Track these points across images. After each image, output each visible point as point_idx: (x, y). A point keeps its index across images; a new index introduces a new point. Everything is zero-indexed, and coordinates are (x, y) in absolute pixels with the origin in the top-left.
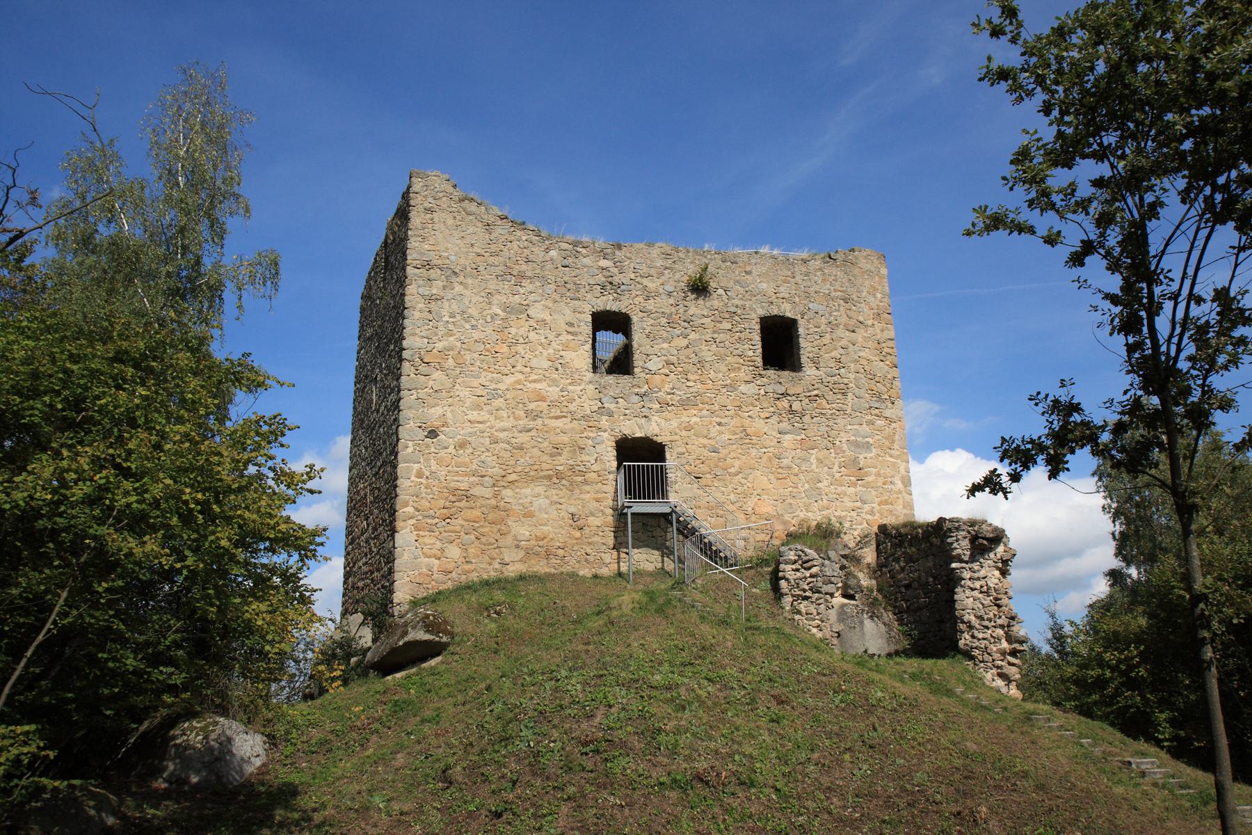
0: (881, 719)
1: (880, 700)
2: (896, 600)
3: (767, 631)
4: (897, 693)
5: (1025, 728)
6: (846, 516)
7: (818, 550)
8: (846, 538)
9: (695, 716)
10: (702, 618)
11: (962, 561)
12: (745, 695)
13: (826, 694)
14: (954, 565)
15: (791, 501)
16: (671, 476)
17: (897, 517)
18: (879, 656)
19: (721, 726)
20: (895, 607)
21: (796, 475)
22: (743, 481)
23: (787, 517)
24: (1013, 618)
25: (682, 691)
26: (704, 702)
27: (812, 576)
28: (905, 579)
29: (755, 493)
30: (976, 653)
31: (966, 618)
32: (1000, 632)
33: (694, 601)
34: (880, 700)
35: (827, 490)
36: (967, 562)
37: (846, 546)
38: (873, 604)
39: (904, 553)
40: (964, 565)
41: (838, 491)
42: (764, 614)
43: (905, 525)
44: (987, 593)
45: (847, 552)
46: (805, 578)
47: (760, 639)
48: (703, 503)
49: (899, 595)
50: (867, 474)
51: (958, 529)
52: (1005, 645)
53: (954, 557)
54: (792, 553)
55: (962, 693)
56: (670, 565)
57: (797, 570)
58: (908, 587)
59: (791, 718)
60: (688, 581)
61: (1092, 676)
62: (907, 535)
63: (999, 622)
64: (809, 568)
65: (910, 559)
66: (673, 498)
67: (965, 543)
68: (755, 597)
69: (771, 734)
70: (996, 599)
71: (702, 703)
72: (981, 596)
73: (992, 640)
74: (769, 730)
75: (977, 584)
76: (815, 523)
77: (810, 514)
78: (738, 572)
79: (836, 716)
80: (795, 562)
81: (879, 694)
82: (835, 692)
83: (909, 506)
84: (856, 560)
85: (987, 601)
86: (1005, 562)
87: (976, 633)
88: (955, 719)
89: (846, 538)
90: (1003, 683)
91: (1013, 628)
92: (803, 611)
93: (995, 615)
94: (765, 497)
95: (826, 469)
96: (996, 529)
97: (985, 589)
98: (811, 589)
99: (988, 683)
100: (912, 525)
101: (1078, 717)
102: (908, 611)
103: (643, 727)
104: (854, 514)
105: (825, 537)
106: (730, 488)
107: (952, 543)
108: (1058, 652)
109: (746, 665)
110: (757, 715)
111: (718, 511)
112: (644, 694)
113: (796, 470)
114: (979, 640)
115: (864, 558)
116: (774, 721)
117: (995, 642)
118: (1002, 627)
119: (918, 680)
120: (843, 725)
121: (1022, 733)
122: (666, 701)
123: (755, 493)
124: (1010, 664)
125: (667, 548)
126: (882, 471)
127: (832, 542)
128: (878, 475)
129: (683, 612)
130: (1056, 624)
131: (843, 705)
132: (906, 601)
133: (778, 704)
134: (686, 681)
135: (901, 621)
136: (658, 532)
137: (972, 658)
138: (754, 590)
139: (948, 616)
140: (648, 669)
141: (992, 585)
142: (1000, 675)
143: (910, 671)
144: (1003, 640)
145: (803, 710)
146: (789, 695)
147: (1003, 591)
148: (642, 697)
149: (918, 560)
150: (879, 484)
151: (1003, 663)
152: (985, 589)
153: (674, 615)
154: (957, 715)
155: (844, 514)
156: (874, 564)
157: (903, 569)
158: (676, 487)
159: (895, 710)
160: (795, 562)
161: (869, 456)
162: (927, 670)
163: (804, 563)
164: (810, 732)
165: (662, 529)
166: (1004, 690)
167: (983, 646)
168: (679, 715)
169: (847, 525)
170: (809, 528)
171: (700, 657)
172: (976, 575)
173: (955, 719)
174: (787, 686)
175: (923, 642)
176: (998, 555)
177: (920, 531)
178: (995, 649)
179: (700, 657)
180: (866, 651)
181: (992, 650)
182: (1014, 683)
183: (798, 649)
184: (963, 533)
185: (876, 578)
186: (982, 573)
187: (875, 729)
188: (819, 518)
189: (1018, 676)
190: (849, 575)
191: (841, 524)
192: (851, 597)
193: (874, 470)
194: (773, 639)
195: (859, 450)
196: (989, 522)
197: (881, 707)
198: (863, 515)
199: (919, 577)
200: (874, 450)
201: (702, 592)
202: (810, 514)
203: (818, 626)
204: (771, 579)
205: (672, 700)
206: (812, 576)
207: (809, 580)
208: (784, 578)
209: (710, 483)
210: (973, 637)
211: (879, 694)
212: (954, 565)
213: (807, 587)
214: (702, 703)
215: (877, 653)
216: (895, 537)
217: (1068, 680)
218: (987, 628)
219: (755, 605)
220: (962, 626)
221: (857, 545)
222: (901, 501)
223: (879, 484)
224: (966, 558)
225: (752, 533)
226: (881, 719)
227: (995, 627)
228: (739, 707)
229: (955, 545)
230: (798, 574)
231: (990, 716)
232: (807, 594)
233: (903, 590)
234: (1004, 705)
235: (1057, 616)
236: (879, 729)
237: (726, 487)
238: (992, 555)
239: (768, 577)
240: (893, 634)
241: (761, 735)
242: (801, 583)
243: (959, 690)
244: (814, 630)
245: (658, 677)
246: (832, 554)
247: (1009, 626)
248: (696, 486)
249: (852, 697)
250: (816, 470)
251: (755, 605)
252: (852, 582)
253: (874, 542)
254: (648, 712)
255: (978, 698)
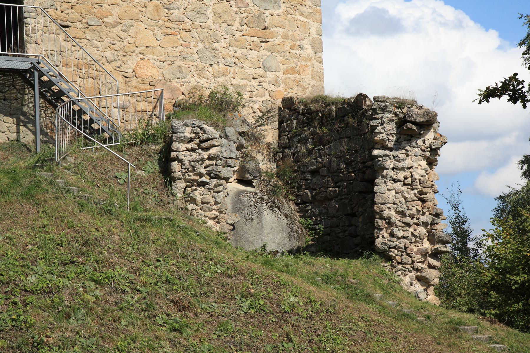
0: (296, 327)
1: (293, 306)
2: (299, 187)
3: (159, 222)
4: (313, 298)
5: (452, 340)
6: (245, 85)
7: (215, 125)
8: (244, 112)
9: (83, 325)
10: (81, 205)
11: (385, 148)
12: (139, 299)
13: (232, 298)
14: (376, 152)
15: (181, 63)
16: (30, 22)
17: (304, 89)
18: (283, 253)
19: (115, 337)
20: (297, 196)
21: (188, 31)
22: (123, 35)
23: (176, 83)
24: (437, 215)
25: (65, 295)
26: (92, 309)
27: (210, 158)
28: (312, 164)
29: (138, 50)
30: (394, 253)
31: (386, 213)
32: (422, 230)
33: (67, 184)
34: (293, 306)
35: (225, 52)
36: (391, 149)
37: (244, 121)
38: (274, 191)
39: (313, 133)
40: (387, 152)
41: (237, 55)
42: (151, 202)
43: (315, 100)
44: (411, 186)
45: (245, 129)
46: (203, 160)
47: (152, 233)
48: (70, 60)
49: (303, 183)
50: (273, 35)
51: (383, 110)
52: (426, 245)
53: (376, 143)
54: (188, 129)
55: (381, 298)
56: (27, 137)
57: (193, 150)
58: (314, 173)
59: (195, 328)
60: (58, 159)
61: (516, 282)
62: (317, 112)
63: (423, 219)
64: (207, 149)
65: (319, 141)
66: (31, 50)
67: (391, 127)
68: (141, 181)
69: (173, 345)
70: (421, 193)
71: (90, 310)
72: (404, 188)
73: (413, 240)
74: (171, 341)
75: (401, 175)
76: (208, 92)
77: (203, 81)
78: (120, 150)
79: (245, 325)
80: (191, 140)
81: (293, 299)
82: (243, 296)
83: (319, 76)
84: (255, 139)
85: (411, 195)
86: (434, 151)
87: (396, 231)
88: (378, 329)
89: (244, 112)
90: (422, 288)
91: (436, 227)
92: (199, 199)
93: (418, 211)
94: (150, 56)
95: (224, 25)
96: (427, 113)
97: (409, 180)
98: (209, 174)
99: (405, 288)
100: (325, 101)
101: (506, 328)
102: (313, 201)
103: (20, 340)
104: (254, 83)
105: (220, 110)
106: (106, 43)
107: (376, 127)
108: (459, 249)
109: (138, 264)
110: (155, 323)
111: (90, 70)
112: (17, 300)
113: (189, 24)
114: (399, 238)
115: (264, 136)
116: (176, 330)
117: (416, 242)
118: (425, 224)
119: (332, 284)
120: (253, 334)
121: (450, 346)
122: (45, 308)
123: (138, 50)
124: (431, 267)
125: (24, 114)
126: (290, 33)
127: (229, 115)
128: (286, 36)
129: (57, 199)
130: (458, 217)
131: (253, 311)
132: (312, 190)
133: (179, 310)
134: (67, 282)
135: (304, 214)
136: (12, 93)
137: (389, 259)
138: (139, 172)
139: (360, 210)
140: (19, 269)
141: (417, 177)
142: (420, 279)
143: (322, 272)
144: (425, 240)
145: (207, 317)
146: (191, 300)
147: (429, 184)
148: (15, 303)
149: (329, 142)
150: (287, 48)
151: (424, 266)
152: (409, 180)
153: (45, 201)
154: (379, 324)
155: (243, 82)
156: (275, 145)
157: (310, 152)
158: (38, 36)
159: (310, 318)
160: (191, 140)
161: (276, 12)
162: (342, 271)
163: (202, 142)
164: (218, 343)
165: (18, 90)
166: (422, 296)
167: (402, 245)
168: (64, 324)
169: (246, 96)
170: (200, 98)
171: (83, 254)
172: (400, 165)
173: (378, 329)
174: (187, 289)
175: (328, 238)
176: (426, 142)
177: (334, 108)
178: (415, 249)
179: (83, 254)
180: (264, 247)
181: (412, 250)
182: (432, 288)
183: (198, 245)
184: (390, 116)
185: (276, 161)
186: (408, 162)
187: (290, 340)
188: (213, 86)
189: (437, 281)
190: (246, 156)
191: (239, 94)
192: (248, 183)
193: (281, 31)
194: (168, 232)
195: (266, 4)
196: (420, 103)
197: (295, 314)
198: (265, 85)
199: (330, 162)
200: (283, 6)
201: (75, 173)
202: (203, 81)
203: (216, 218)
204: (160, 160)
205: (53, 306)
206: (210, 158)
207: (207, 162)
208: (177, 159)
209: (80, 34)
210: (392, 235)
211: (293, 299)
212: (376, 152)
213: (204, 171)
214: (90, 310)
215: (281, 250)
216: (303, 114)
217: (485, 285)
218: (409, 225)
219: (140, 190)
220: (381, 223)
221: (257, 121)
222: (309, 70)
223: (287, 48)
224: (391, 145)
225: (132, 100)
226: (296, 327)
227: (417, 224)
228: (134, 314)
229: (379, 129)
230: (195, 155)
231: (414, 326)
232: (204, 179)
233: (309, 176)
234: (426, 313)
235: (460, 208)
236: (295, 339)
237: (101, 40)
238: (420, 142)
239: (156, 157)
240: (295, 228)
241: (162, 347)
242: (197, 165)
243: (378, 295)
244: (211, 223)
245: (33, 279)
246: (230, 131)
247: (432, 224)
248: (63, 36)
249: (262, 302)
250: (213, 27)
251: (140, 190)
252: (250, 165)
253: (276, 118)
254: (25, 322)
255: (398, 305)
